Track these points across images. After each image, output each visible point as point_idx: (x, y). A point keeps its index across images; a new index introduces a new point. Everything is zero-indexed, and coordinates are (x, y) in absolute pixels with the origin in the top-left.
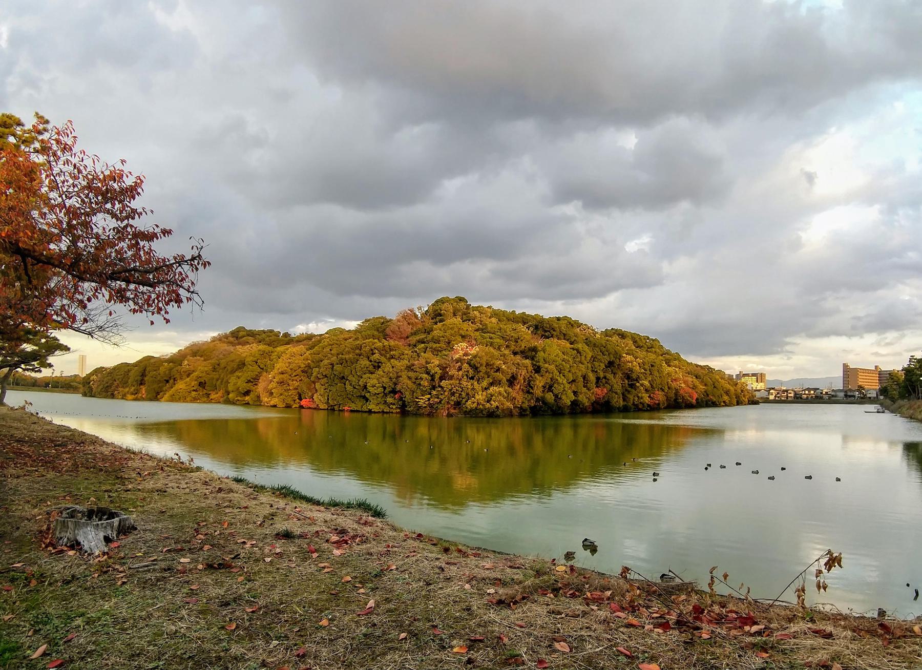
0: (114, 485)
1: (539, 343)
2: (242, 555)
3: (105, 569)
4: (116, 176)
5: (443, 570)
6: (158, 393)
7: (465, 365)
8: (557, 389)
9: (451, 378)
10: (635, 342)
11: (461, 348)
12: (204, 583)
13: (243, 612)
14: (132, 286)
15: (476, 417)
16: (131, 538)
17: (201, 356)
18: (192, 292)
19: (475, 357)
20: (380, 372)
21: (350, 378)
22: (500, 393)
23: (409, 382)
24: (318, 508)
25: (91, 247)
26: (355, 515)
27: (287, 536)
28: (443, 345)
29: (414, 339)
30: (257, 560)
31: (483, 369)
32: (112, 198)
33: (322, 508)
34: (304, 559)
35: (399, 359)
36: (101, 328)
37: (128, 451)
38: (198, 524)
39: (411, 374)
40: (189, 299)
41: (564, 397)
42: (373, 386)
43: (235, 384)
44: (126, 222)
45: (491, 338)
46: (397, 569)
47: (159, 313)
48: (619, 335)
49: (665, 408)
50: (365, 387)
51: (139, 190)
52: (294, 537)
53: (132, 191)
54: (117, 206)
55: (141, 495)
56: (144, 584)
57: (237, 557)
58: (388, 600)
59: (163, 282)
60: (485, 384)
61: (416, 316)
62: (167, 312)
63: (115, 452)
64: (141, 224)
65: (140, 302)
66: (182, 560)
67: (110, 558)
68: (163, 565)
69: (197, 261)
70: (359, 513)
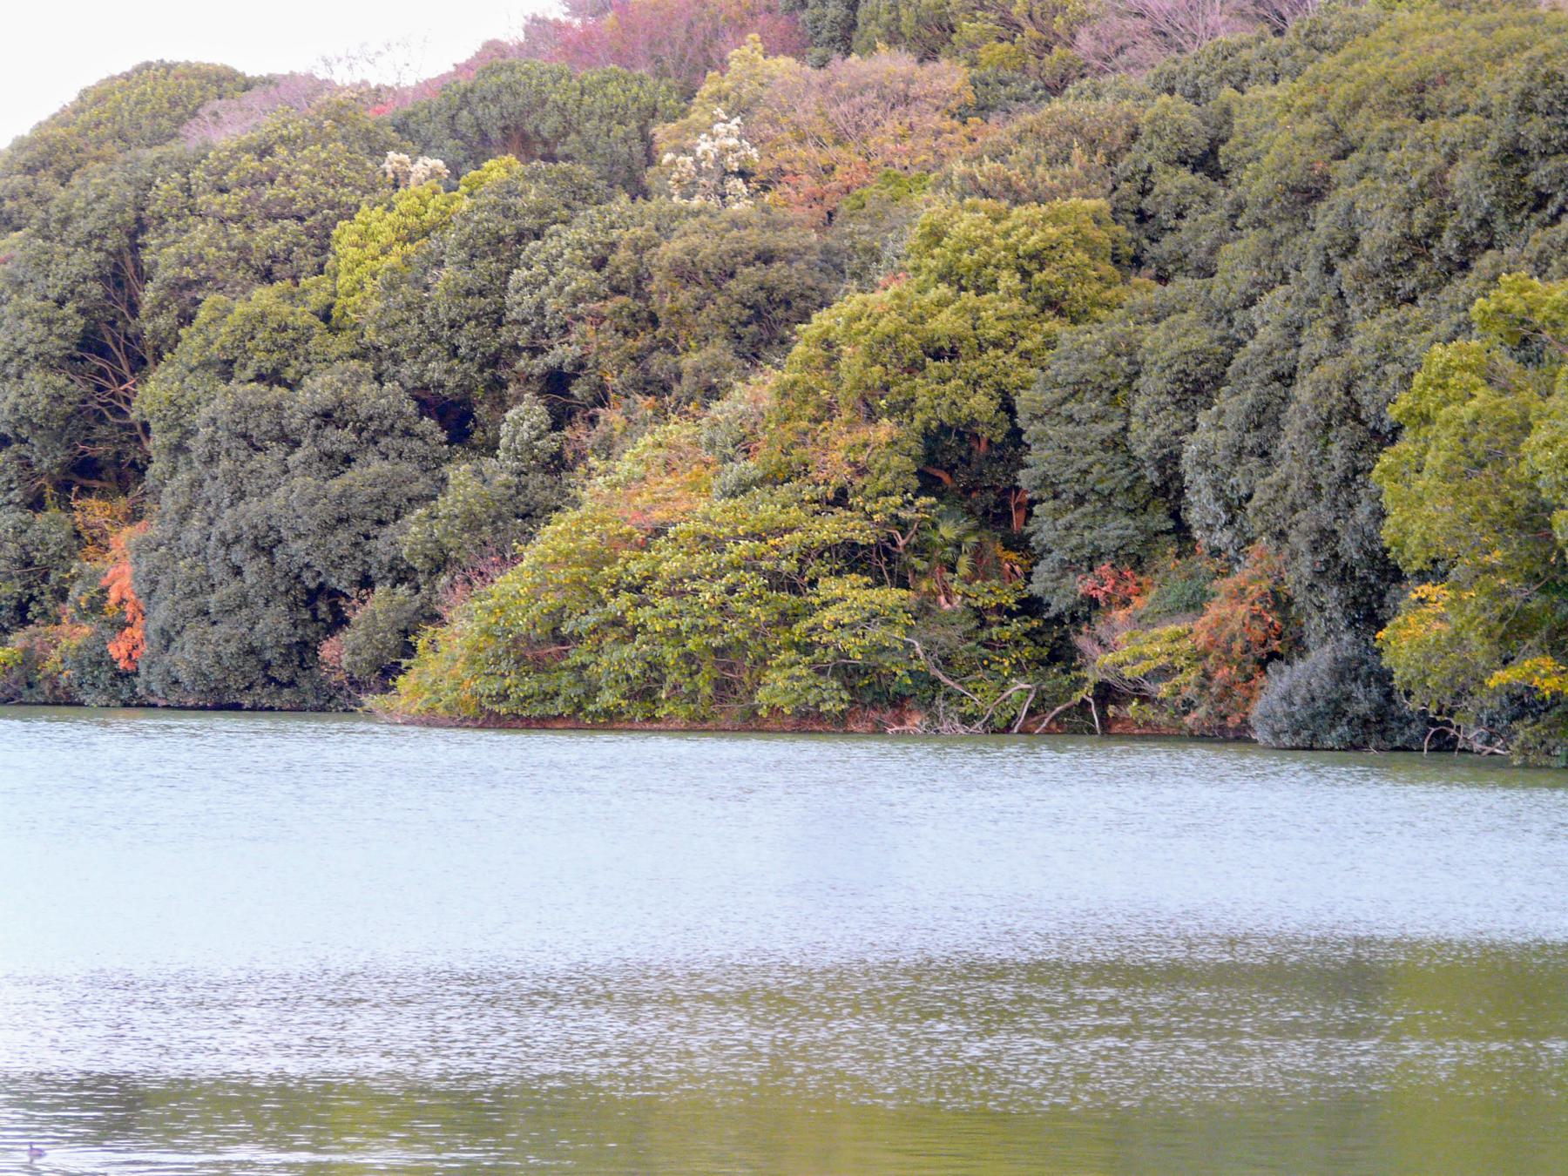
6: (323, 607)
49: (1264, 748)
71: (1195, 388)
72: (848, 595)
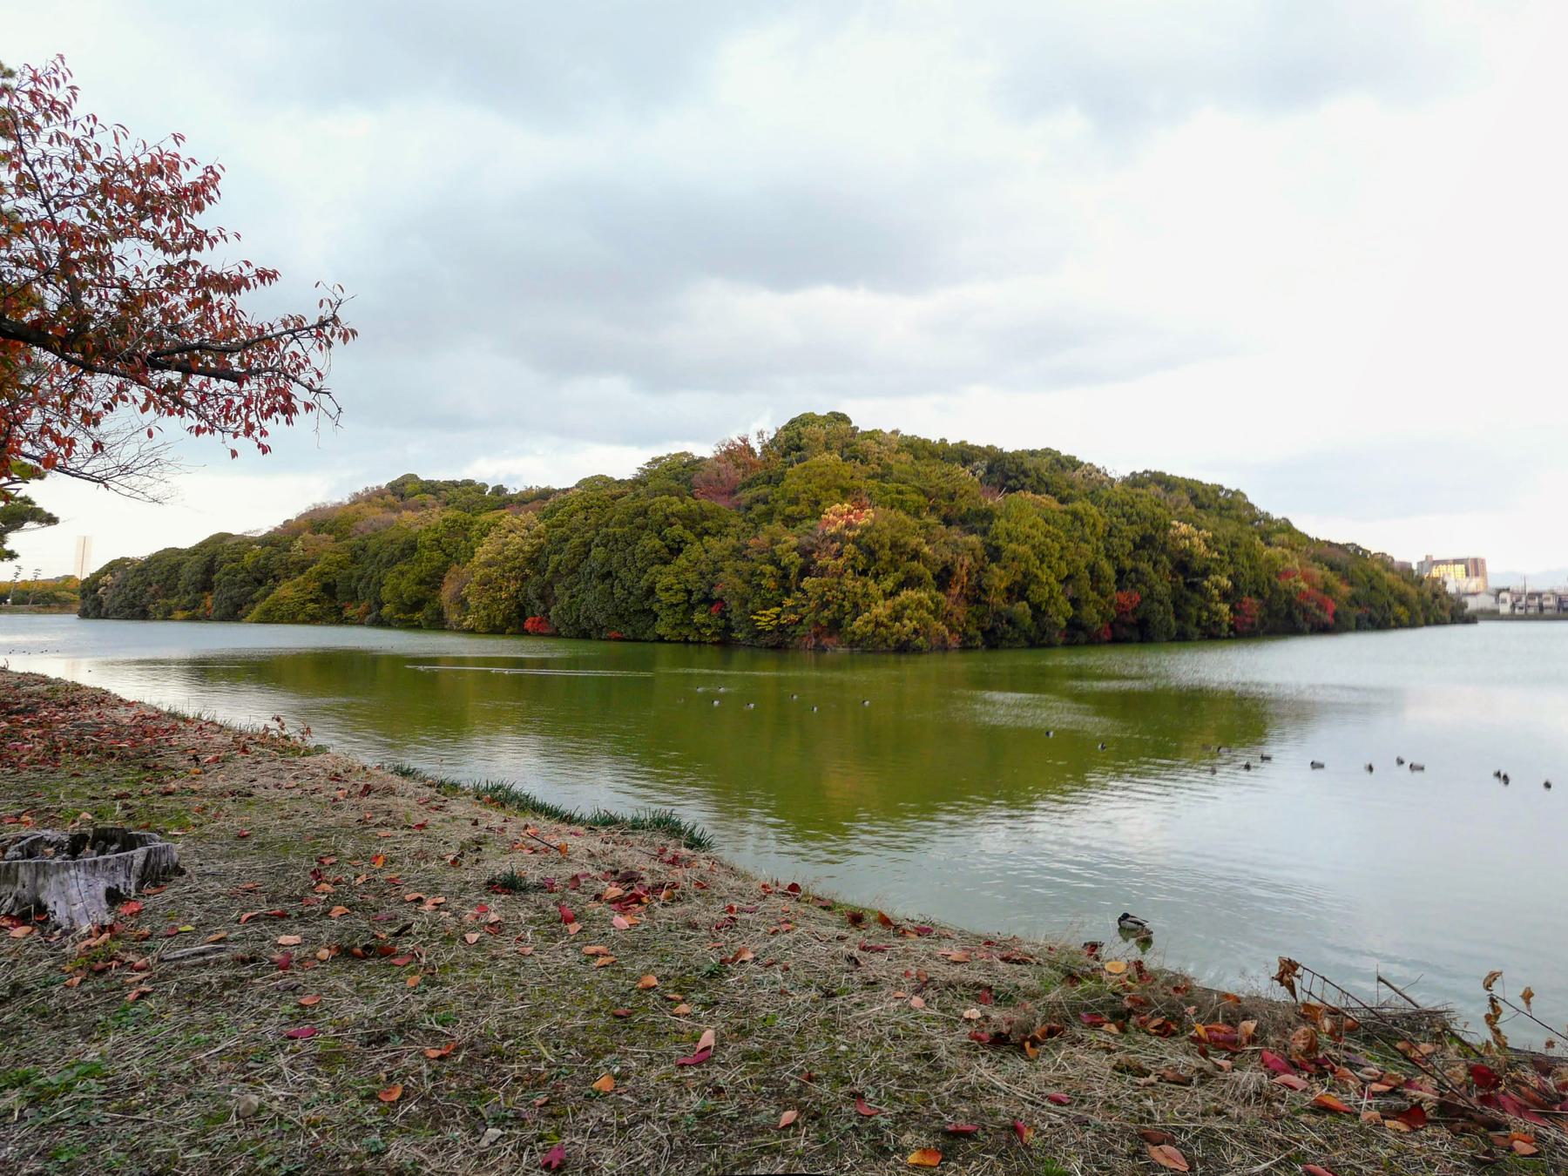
0: (138, 783)
1: (994, 501)
2: (416, 928)
3: (101, 964)
4: (163, 166)
5: (857, 963)
6: (239, 607)
7: (850, 547)
8: (1038, 594)
9: (823, 571)
10: (1194, 498)
11: (836, 516)
12: (330, 990)
13: (415, 1058)
14: (196, 380)
15: (875, 651)
16: (169, 893)
17: (330, 532)
18: (318, 391)
19: (868, 529)
20: (681, 561)
21: (622, 573)
22: (920, 604)
23: (737, 581)
24: (573, 828)
25: (111, 303)
26: (652, 844)
27: (510, 885)
28: (803, 507)
29: (746, 496)
30: (449, 939)
31: (886, 554)
32: (154, 210)
33: (581, 829)
34: (552, 937)
35: (719, 533)
36: (125, 470)
37: (173, 716)
38: (320, 861)
39: (741, 565)
40: (308, 407)
41: (1051, 610)
42: (667, 590)
43: (395, 588)
44: (183, 255)
45: (900, 492)
46: (756, 959)
47: (248, 433)
48: (1159, 483)
50: (651, 591)
51: (212, 193)
52: (524, 889)
53: (198, 195)
54: (166, 223)
55: (197, 803)
56: (192, 997)
57: (404, 931)
58: (743, 1032)
59: (258, 372)
60: (889, 584)
61: (752, 451)
62: (264, 433)
63: (144, 717)
64: (214, 259)
65: (210, 412)
66: (283, 939)
67: (115, 938)
68: (240, 950)
69: (327, 329)
70: (660, 840)
71: (360, 579)
72: (311, 606)
